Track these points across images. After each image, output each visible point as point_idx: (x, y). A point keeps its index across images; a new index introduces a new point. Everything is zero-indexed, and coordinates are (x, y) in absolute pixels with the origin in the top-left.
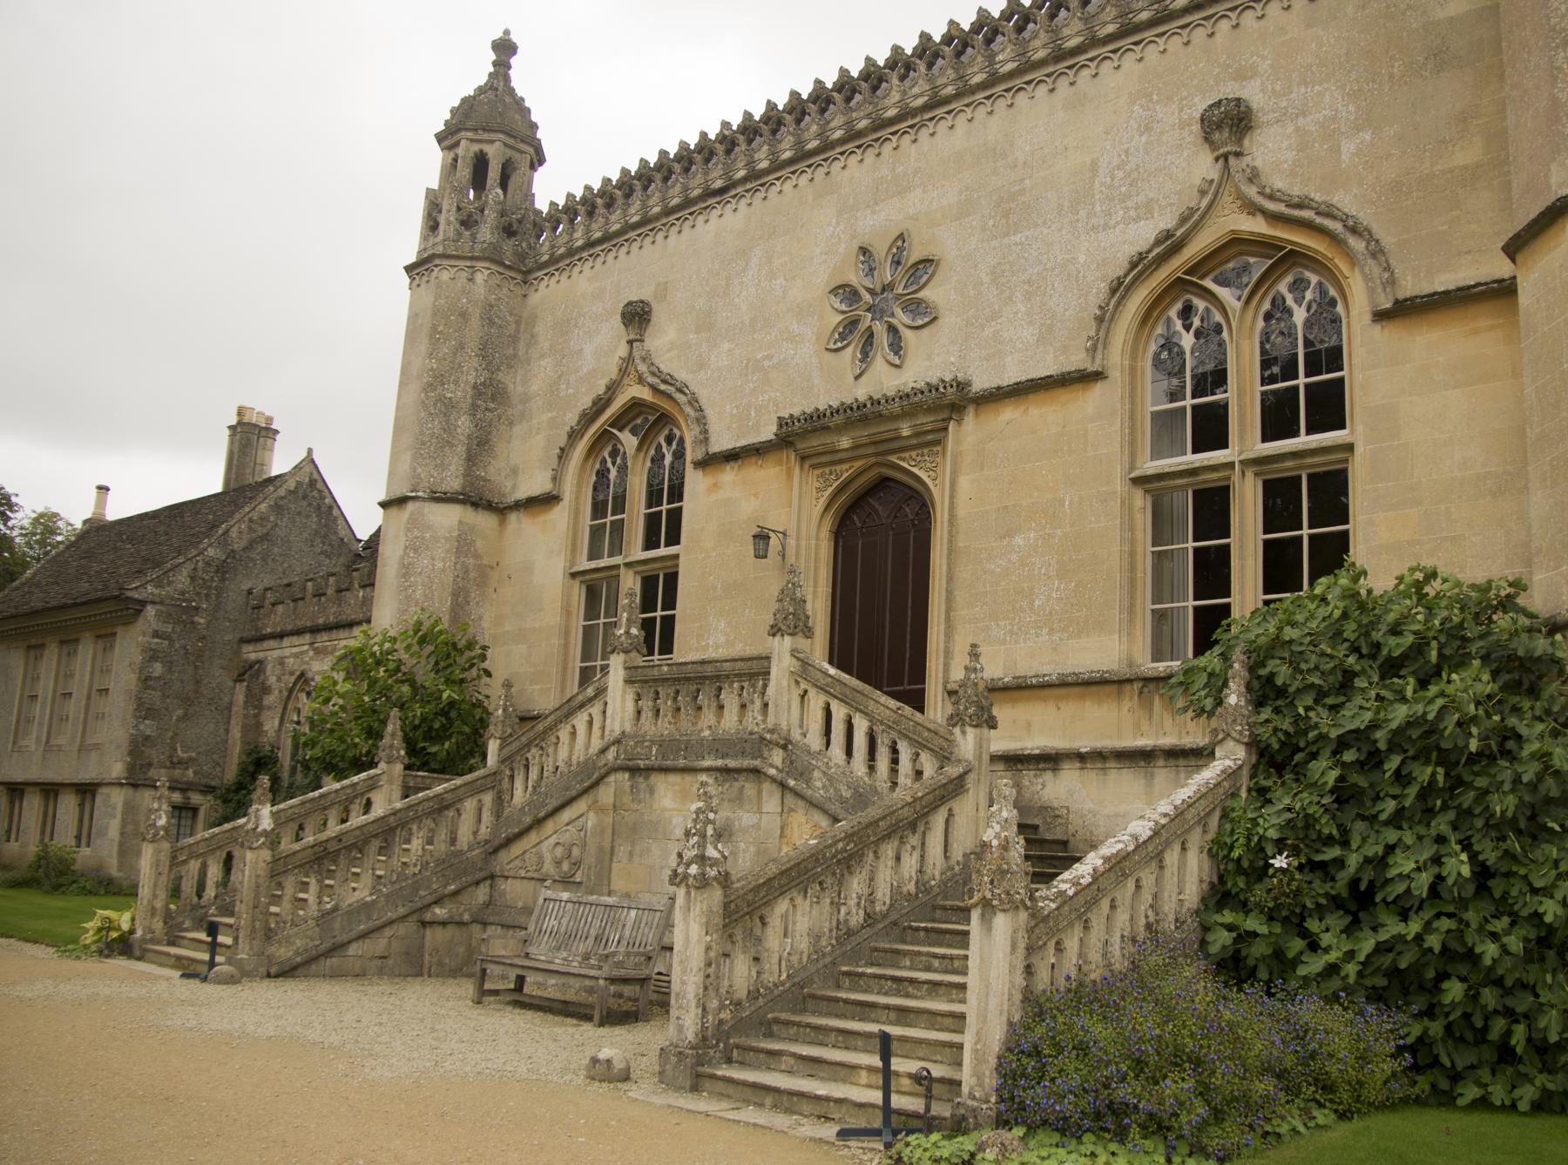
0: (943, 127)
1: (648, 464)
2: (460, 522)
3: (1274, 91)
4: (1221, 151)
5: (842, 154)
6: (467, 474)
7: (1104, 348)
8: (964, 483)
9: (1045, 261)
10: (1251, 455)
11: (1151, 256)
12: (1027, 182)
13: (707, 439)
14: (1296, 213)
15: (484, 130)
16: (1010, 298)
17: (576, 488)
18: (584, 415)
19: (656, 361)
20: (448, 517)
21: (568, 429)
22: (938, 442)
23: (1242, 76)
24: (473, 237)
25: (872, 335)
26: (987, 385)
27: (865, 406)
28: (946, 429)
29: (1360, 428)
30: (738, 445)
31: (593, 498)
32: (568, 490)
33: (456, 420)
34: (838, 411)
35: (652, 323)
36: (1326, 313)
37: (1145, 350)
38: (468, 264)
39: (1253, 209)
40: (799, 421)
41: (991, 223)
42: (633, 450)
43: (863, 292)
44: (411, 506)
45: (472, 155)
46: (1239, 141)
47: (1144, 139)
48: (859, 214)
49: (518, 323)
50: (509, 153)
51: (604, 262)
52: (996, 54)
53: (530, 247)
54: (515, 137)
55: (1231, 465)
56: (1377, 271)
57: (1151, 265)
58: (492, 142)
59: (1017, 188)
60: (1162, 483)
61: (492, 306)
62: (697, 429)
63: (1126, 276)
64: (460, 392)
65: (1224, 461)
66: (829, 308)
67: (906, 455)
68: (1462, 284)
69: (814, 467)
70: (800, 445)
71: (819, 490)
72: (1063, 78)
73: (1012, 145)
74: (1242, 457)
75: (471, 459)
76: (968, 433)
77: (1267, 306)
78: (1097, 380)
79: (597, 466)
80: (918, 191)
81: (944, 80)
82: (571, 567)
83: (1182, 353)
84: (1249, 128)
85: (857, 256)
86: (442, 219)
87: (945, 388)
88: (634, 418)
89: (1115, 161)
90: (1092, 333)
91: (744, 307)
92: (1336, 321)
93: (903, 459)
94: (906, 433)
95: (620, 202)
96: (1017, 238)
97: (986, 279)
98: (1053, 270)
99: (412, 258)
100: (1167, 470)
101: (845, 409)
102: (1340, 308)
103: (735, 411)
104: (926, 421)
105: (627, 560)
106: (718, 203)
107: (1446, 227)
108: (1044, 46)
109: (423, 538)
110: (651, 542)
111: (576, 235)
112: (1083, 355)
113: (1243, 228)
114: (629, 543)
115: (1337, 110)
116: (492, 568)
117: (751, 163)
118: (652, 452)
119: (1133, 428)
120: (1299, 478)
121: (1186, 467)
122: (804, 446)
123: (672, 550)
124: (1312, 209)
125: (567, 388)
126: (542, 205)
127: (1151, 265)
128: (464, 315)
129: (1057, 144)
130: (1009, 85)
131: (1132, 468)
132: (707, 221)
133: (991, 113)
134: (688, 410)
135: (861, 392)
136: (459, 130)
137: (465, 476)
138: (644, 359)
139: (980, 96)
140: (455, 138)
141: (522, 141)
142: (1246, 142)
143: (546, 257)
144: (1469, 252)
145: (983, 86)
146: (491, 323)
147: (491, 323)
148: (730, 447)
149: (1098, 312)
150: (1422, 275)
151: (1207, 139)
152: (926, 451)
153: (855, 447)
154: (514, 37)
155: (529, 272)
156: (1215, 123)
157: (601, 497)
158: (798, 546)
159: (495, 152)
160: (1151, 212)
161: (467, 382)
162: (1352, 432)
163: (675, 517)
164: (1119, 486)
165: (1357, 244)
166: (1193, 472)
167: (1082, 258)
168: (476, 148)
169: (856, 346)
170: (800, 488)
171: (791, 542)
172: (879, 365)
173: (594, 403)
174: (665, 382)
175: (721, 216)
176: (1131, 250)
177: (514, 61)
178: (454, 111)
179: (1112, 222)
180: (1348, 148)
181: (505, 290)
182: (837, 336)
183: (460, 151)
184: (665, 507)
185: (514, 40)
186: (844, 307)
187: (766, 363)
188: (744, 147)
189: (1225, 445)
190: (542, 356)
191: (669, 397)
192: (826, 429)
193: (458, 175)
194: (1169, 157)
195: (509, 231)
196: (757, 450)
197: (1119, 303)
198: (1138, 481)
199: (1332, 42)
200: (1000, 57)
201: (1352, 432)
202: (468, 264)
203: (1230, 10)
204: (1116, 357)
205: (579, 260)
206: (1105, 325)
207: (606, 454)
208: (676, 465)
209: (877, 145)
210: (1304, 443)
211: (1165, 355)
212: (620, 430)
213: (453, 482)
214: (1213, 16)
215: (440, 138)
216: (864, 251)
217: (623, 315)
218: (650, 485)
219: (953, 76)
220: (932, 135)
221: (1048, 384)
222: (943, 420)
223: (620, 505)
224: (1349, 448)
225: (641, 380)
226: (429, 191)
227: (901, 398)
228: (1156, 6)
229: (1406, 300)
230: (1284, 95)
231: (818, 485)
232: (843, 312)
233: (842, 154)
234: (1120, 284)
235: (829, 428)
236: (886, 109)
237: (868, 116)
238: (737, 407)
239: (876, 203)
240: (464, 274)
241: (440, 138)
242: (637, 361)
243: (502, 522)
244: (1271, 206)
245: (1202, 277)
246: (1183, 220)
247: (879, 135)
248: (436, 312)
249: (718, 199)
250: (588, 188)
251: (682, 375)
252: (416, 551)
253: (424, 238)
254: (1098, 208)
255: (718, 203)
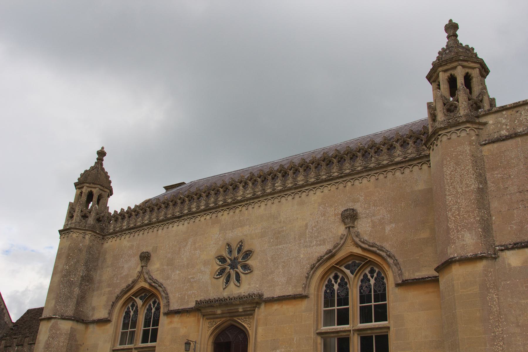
0: (256, 206)
1: (146, 311)
2: (71, 328)
3: (364, 207)
4: (347, 226)
5: (222, 210)
6: (76, 309)
7: (308, 288)
8: (260, 330)
9: (289, 255)
10: (356, 328)
11: (324, 258)
12: (284, 228)
13: (169, 305)
14: (371, 248)
15: (93, 183)
16: (278, 267)
17: (118, 317)
18: (123, 291)
19: (151, 274)
20: (66, 326)
21: (116, 295)
22: (252, 314)
23: (355, 201)
24: (86, 221)
25: (230, 274)
26: (269, 296)
27: (227, 300)
28: (255, 310)
29: (392, 322)
30: (180, 308)
31: (124, 322)
32: (114, 318)
33: (74, 289)
34: (217, 301)
35: (151, 260)
36: (381, 281)
37: (321, 290)
38: (84, 232)
39: (358, 246)
40: (203, 303)
41: (272, 240)
42: (141, 306)
43: (228, 259)
44: (53, 321)
45: (87, 192)
46: (353, 223)
47: (323, 218)
48: (227, 232)
49: (99, 253)
50: (101, 192)
51: (134, 236)
52: (276, 183)
53: (106, 226)
54: (103, 187)
55: (350, 331)
56: (397, 270)
57: (324, 261)
58: (95, 188)
59: (281, 230)
60: (327, 335)
61: (91, 247)
62: (165, 301)
63: (316, 264)
64: (75, 278)
65: (348, 329)
66: (215, 263)
67: (240, 318)
68: (423, 277)
69: (207, 319)
70: (203, 311)
71: (209, 327)
72: (297, 194)
73: (280, 215)
74: (353, 328)
75: (78, 304)
76: (262, 312)
77: (362, 277)
78: (306, 298)
79: (126, 310)
80: (248, 226)
81: (258, 190)
82: (113, 347)
83: (334, 290)
84: (356, 219)
85: (226, 246)
86: (75, 215)
87: (255, 296)
88: (141, 294)
89: (313, 225)
90: (305, 282)
91: (185, 259)
92: (384, 284)
93: (239, 319)
94: (241, 310)
95: (141, 214)
96: (281, 247)
97: (269, 259)
98: (292, 259)
99: (62, 228)
100: (329, 331)
101: (220, 300)
102: (385, 280)
103: (180, 296)
104: (248, 306)
105: (135, 347)
106: (177, 221)
107: (418, 257)
108: (291, 183)
109: (56, 333)
110: (145, 340)
111: (124, 224)
112: (301, 289)
113: (354, 251)
114: (136, 340)
115: (384, 216)
116: (81, 345)
117: (190, 209)
118: (147, 307)
119: (317, 315)
120: (372, 336)
121: (335, 330)
122: (204, 311)
123: (153, 344)
124: (376, 247)
125: (117, 280)
126: (111, 211)
127: (324, 261)
128: (80, 250)
129: (295, 216)
130: (279, 195)
131: (317, 329)
132: (173, 227)
133: (273, 203)
134: (163, 294)
135: (225, 294)
136: (84, 183)
137: (75, 310)
138: (147, 273)
139: (269, 197)
140: (82, 186)
141: (106, 188)
142: (356, 223)
143: (112, 231)
144: (426, 266)
145: (271, 194)
146: (90, 254)
147: (90, 254)
148: (177, 309)
149: (306, 275)
150: (411, 272)
151: (343, 221)
152: (247, 317)
153: (222, 313)
154: (105, 150)
155: (105, 235)
156: (346, 217)
157: (127, 321)
158: (200, 348)
159: (460, 74)
160: (325, 243)
161: (79, 275)
162: (389, 322)
163: (155, 332)
164: (313, 335)
165: (390, 261)
166: (338, 332)
167: (302, 256)
168: (89, 189)
169: (224, 277)
170: (202, 326)
171: (198, 346)
172: (232, 285)
173: (127, 287)
174: (154, 282)
175: (178, 226)
176: (317, 255)
177: (104, 158)
178: (82, 175)
179: (312, 245)
180: (388, 228)
181: (96, 242)
182: (217, 273)
183: (84, 190)
184: (151, 328)
185: (105, 151)
186: (220, 263)
187: (192, 280)
188: (187, 202)
189: (347, 323)
190: (108, 267)
191: (156, 288)
192: (212, 306)
193: (82, 199)
194: (331, 225)
195: (99, 220)
196: (187, 311)
197: (313, 273)
198: (320, 334)
199: (383, 194)
200: (277, 185)
201: (389, 322)
202: (84, 232)
203: (351, 179)
204: (312, 290)
205: (124, 234)
206: (307, 288)
207: (130, 305)
208: (156, 312)
209: (234, 209)
210: (373, 325)
211: (328, 291)
212: (136, 297)
213: (70, 312)
214: (346, 180)
215: (76, 185)
216: (228, 245)
217: (141, 257)
218: (146, 319)
219: (260, 189)
220: (253, 208)
221: (314, 184)
222: (254, 307)
223: (134, 325)
224: (388, 328)
225: (145, 280)
226: (70, 203)
227: (239, 298)
228: (328, 175)
229: (406, 280)
230: (368, 209)
231: (209, 326)
232: (220, 265)
233: (222, 210)
234: (314, 266)
235: (214, 306)
236: (238, 197)
237: (231, 198)
238: (181, 294)
239: (233, 229)
240: (81, 235)
241: (76, 185)
242: (144, 274)
243: (87, 328)
244: (363, 245)
245: (340, 266)
246: (335, 247)
247: (235, 205)
248: (70, 248)
249: (177, 220)
250: (129, 208)
251: (161, 280)
252: (53, 339)
253: (67, 220)
254: (307, 240)
255: (177, 221)
